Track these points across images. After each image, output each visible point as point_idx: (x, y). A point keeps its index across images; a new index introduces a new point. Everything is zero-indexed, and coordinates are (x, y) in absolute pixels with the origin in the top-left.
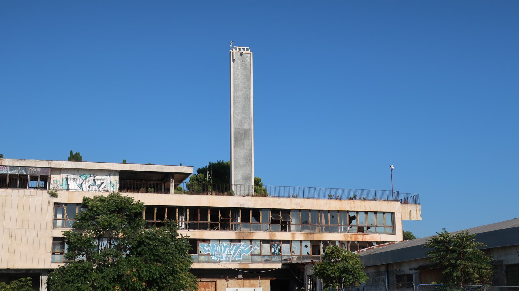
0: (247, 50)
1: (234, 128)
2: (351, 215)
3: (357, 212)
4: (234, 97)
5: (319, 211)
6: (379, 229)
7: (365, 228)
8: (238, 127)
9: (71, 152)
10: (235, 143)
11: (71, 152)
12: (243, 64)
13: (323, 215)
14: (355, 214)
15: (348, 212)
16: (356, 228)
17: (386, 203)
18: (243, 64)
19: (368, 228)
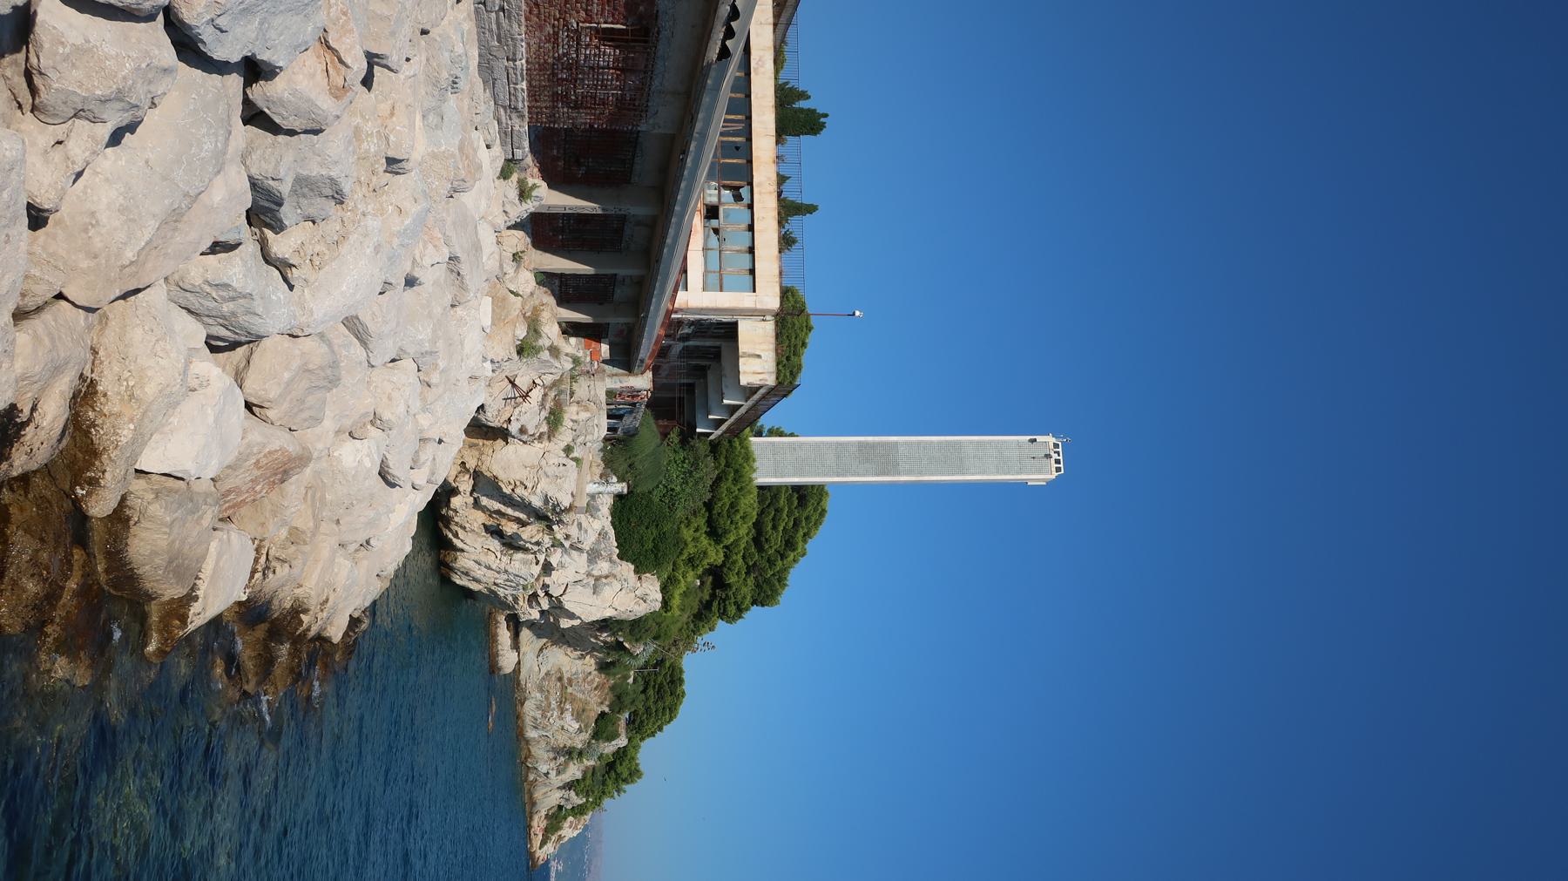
0: (1058, 470)
1: (896, 443)
2: (744, 192)
3: (751, 207)
4: (960, 442)
5: (749, 118)
6: (714, 255)
7: (714, 223)
8: (901, 449)
9: (826, 116)
10: (867, 444)
11: (826, 116)
12: (1027, 460)
13: (740, 127)
14: (746, 201)
15: (751, 184)
16: (714, 200)
17: (777, 272)
18: (1027, 460)
19: (716, 231)
